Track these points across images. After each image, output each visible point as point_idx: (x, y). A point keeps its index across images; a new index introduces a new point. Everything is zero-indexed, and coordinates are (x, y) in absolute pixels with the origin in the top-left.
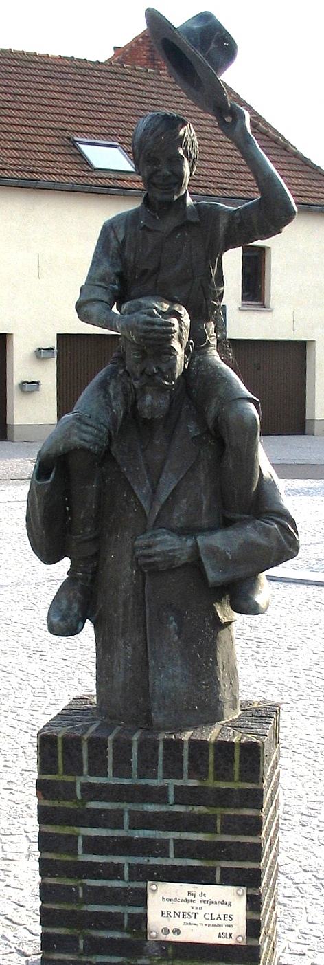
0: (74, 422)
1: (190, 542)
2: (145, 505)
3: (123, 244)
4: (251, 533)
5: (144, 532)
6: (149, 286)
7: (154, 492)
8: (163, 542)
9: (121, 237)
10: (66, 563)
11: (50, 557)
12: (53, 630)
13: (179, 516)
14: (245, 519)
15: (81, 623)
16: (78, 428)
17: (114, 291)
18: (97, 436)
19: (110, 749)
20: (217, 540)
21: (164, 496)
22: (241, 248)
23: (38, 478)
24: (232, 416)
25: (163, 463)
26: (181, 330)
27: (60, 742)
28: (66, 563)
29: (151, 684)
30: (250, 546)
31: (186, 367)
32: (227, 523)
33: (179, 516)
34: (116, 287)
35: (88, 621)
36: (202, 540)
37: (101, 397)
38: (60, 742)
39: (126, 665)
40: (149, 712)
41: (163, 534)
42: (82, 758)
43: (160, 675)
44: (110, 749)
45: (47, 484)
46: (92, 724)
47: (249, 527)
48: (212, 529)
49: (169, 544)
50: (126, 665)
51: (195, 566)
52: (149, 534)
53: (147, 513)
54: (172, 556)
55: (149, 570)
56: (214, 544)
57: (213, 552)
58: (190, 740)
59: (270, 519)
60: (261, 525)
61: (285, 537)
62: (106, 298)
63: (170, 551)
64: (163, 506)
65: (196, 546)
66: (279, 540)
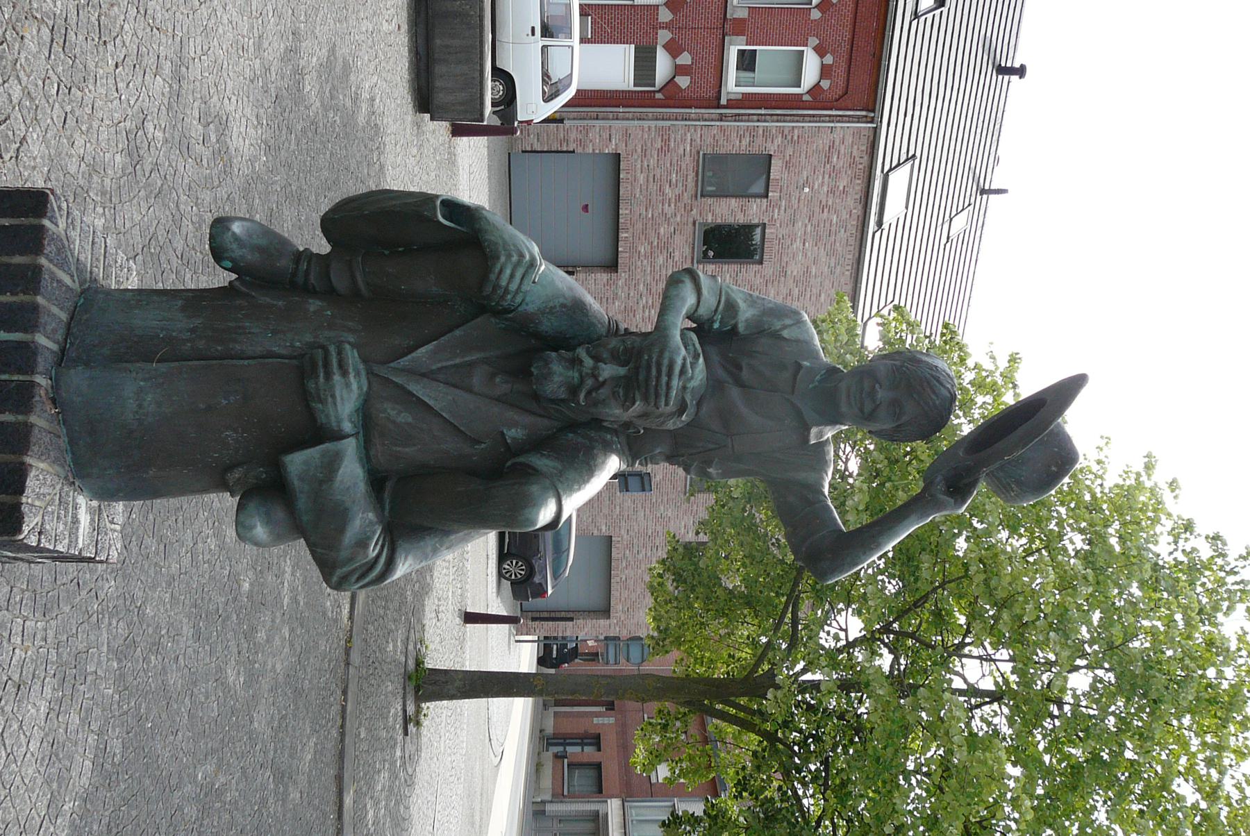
0: (528, 257)
1: (347, 427)
2: (404, 361)
3: (776, 335)
4: (363, 520)
5: (365, 360)
6: (721, 373)
7: (424, 375)
8: (348, 385)
9: (785, 333)
10: (322, 246)
11: (331, 223)
12: (220, 225)
13: (394, 414)
14: (383, 509)
15: (229, 264)
16: (519, 263)
17: (711, 321)
18: (507, 291)
19: (22, 298)
20: (351, 471)
21: (417, 388)
22: (492, 537)
23: (443, 202)
24: (535, 489)
25: (470, 390)
26: (661, 416)
27: (33, 221)
28: (322, 246)
29: (128, 365)
30: (341, 516)
31: (605, 424)
32: (377, 481)
33: (394, 414)
34: (716, 326)
35: (234, 276)
36: (350, 447)
37: (561, 300)
38: (33, 221)
39: (162, 329)
40: (87, 364)
41: (360, 388)
42: (591, 501)
43: (144, 380)
44: (22, 298)
45: (435, 213)
46: (72, 276)
47: (371, 515)
48: (366, 457)
49: (345, 400)
50: (162, 329)
51: (318, 433)
52: (361, 366)
53: (392, 365)
54: (326, 400)
55: (307, 370)
56: (346, 463)
57: (331, 465)
58: (32, 425)
59: (383, 547)
60: (374, 533)
61: (355, 569)
62: (702, 311)
63: (333, 396)
64: (401, 388)
65: (340, 436)
66: (351, 560)
